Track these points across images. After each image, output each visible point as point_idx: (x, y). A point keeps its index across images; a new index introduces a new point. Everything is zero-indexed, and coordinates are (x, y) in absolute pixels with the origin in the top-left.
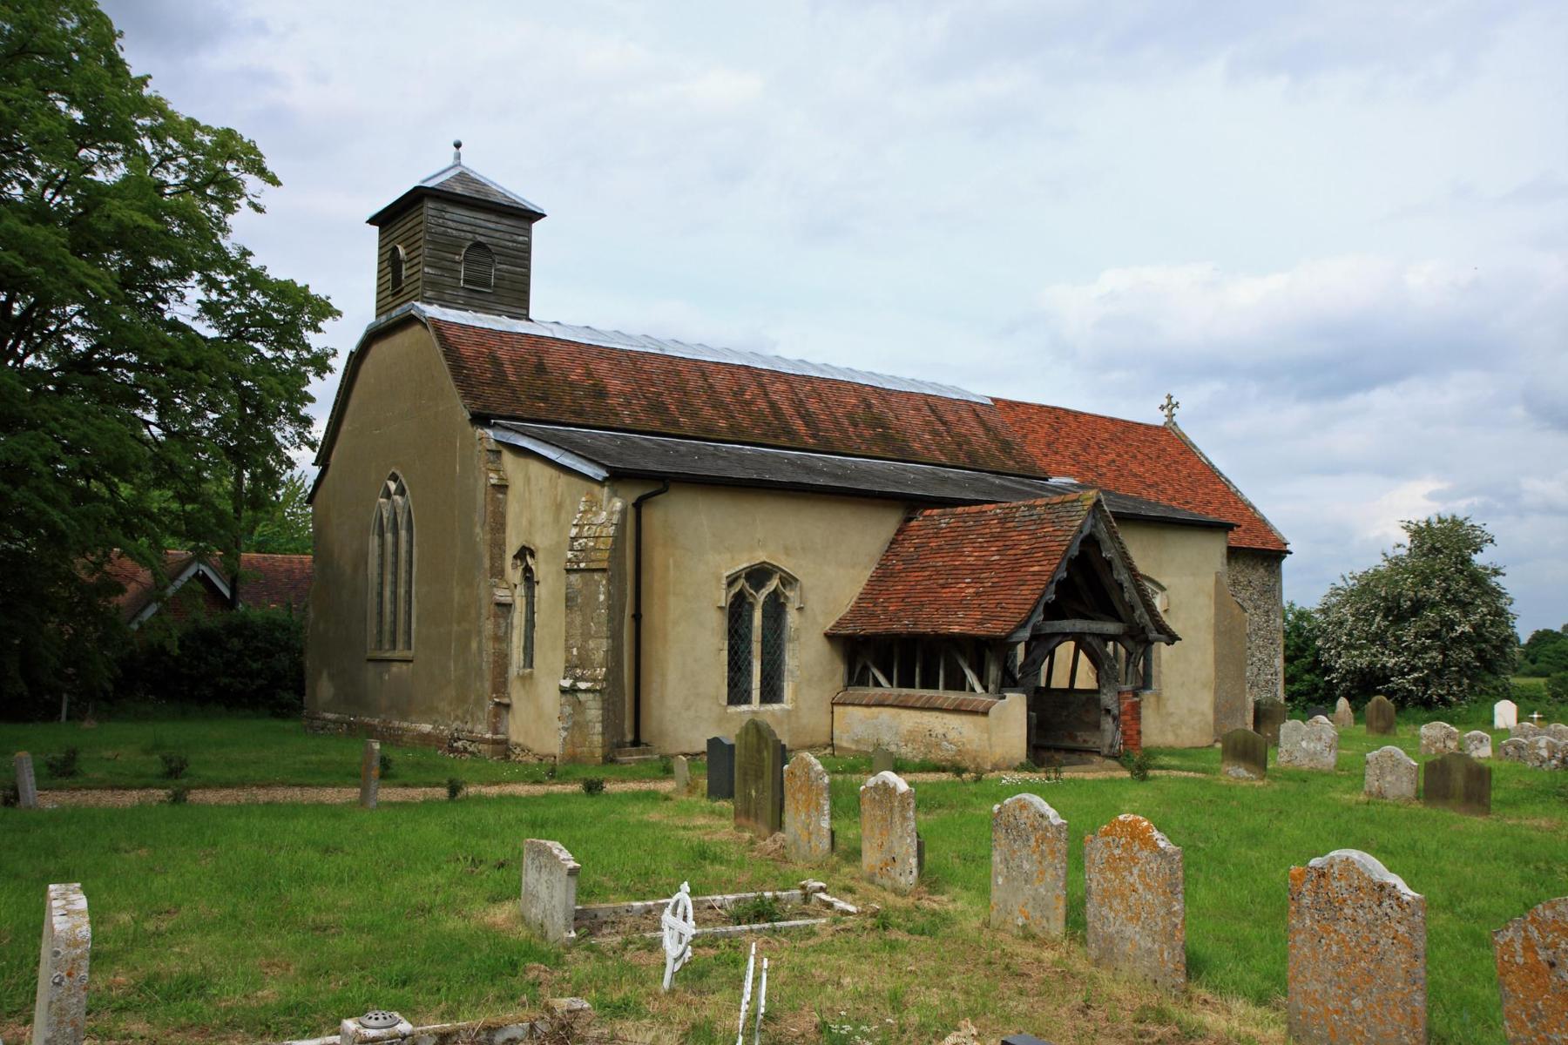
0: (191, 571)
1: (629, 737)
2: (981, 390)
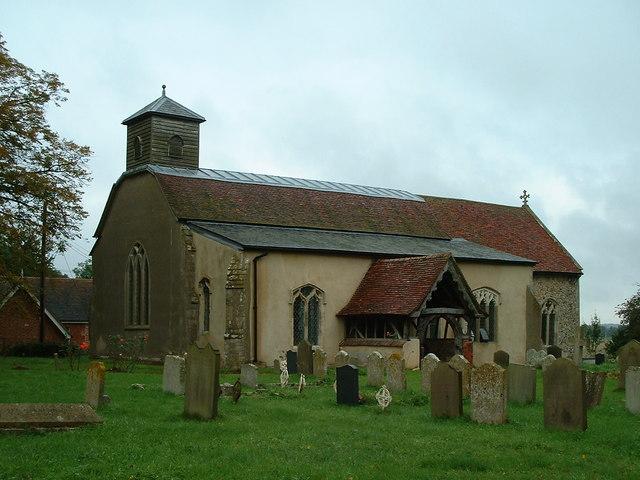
1: (253, 359)
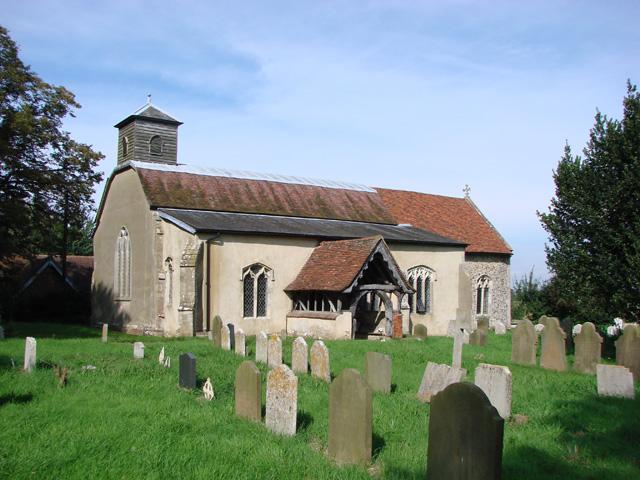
0: (47, 264)
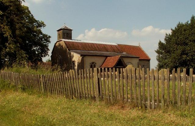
2: (129, 45)
